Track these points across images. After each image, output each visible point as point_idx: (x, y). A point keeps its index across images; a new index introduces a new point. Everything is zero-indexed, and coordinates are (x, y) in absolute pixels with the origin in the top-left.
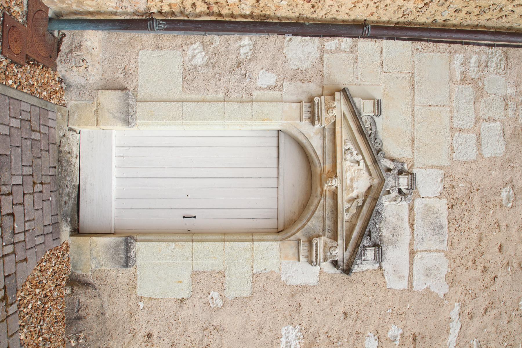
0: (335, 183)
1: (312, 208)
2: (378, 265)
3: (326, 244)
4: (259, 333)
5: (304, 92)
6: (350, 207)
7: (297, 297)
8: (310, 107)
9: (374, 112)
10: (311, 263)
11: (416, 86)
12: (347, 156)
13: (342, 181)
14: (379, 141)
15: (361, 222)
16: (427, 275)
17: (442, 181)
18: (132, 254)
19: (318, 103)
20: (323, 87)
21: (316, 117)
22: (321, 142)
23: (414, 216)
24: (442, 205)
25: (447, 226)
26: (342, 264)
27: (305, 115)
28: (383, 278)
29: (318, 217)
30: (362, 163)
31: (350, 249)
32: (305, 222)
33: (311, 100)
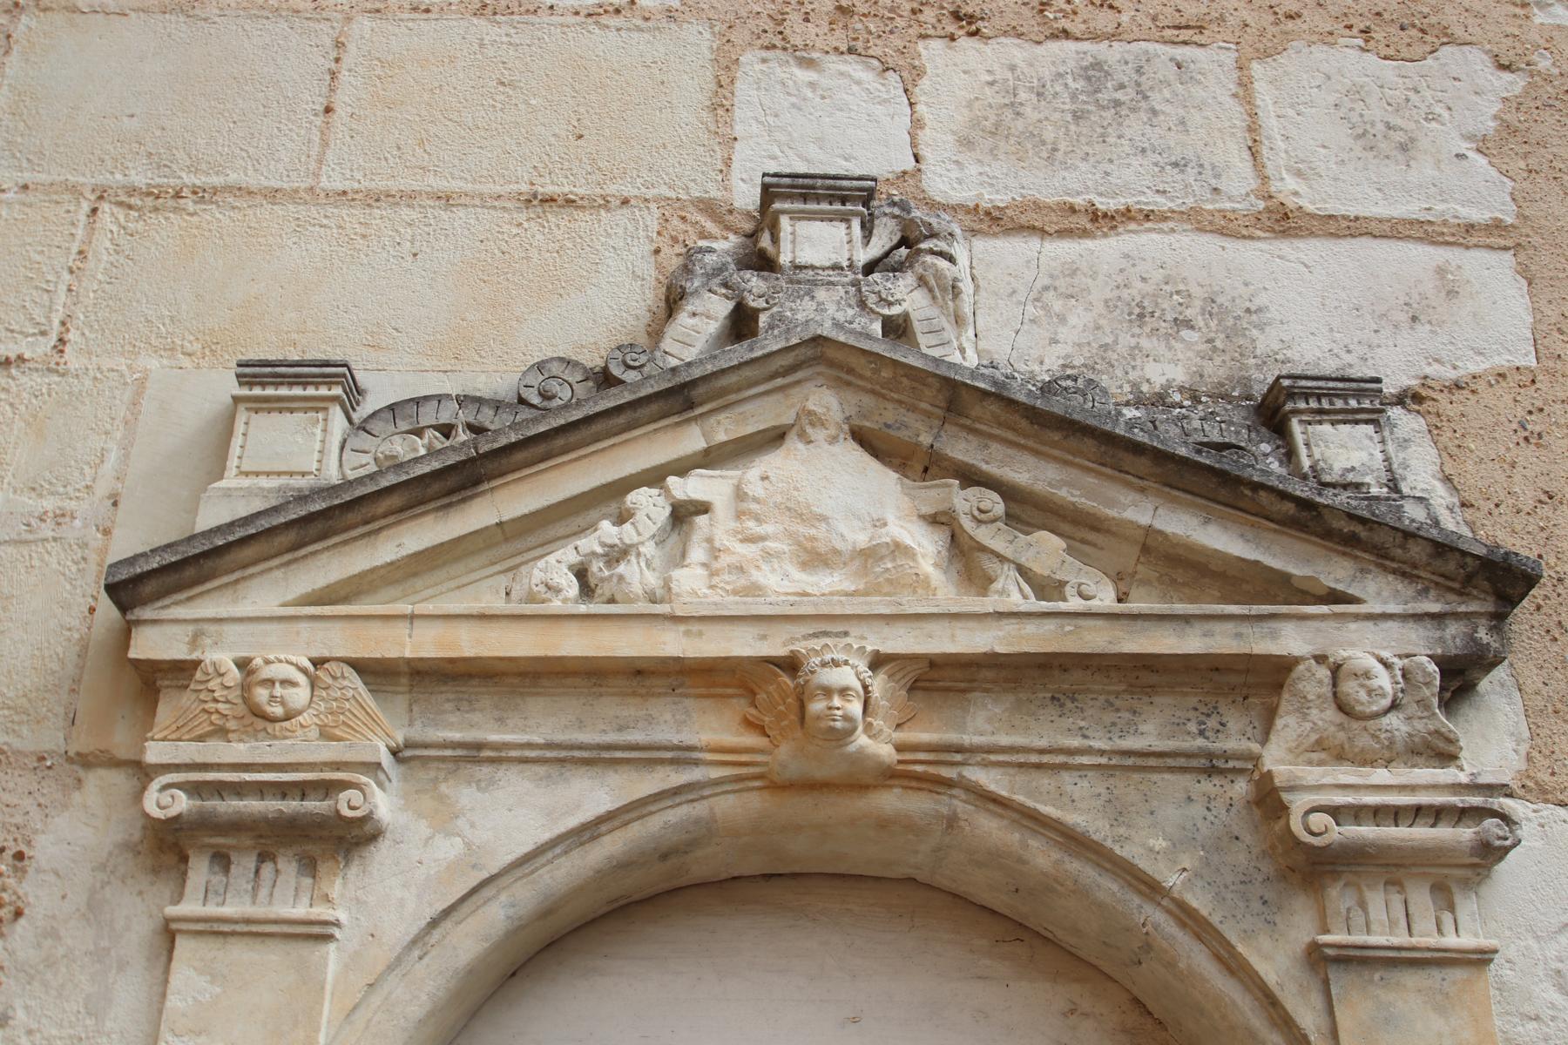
0: (843, 672)
1: (1042, 855)
2: (1395, 412)
3: (1319, 745)
5: (93, 908)
6: (1022, 570)
8: (222, 860)
9: (318, 405)
10: (1489, 854)
11: (189, 179)
12: (637, 589)
13: (829, 622)
14: (535, 379)
15: (1126, 497)
16: (1403, 148)
17: (808, 63)
19: (195, 789)
20: (86, 761)
21: (313, 805)
22: (514, 784)
23: (1037, 206)
25: (1086, 46)
26: (1453, 629)
27: (287, 896)
28: (1481, 386)
29: (1118, 813)
31: (1335, 572)
32: (1159, 917)
33: (168, 847)
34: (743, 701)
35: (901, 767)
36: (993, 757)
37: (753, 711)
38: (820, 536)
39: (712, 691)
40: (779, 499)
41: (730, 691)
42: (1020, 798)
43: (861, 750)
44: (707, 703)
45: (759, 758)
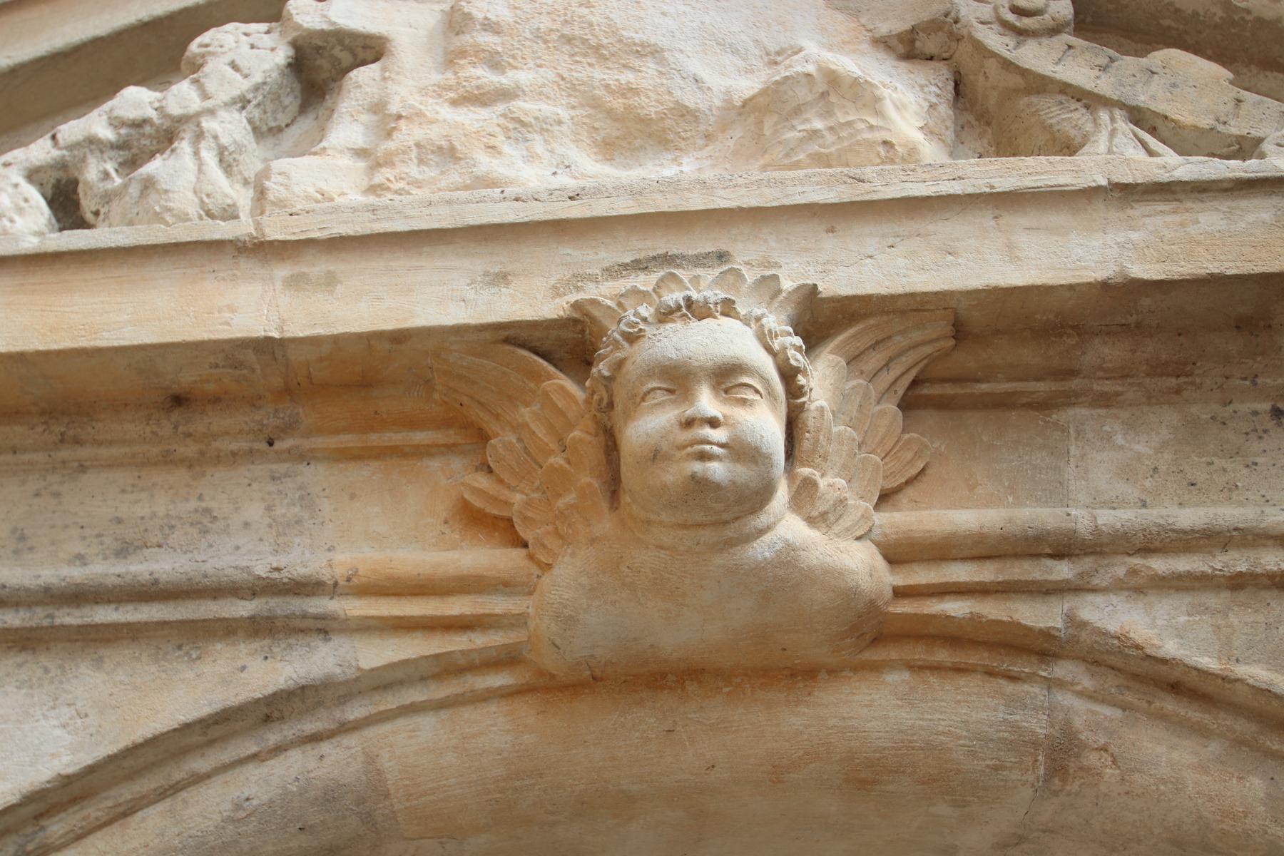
34: (457, 463)
35: (905, 607)
36: (1159, 565)
37: (482, 481)
38: (645, 83)
39: (374, 439)
40: (545, 23)
41: (420, 437)
42: (1256, 672)
43: (788, 558)
44: (360, 473)
45: (498, 605)
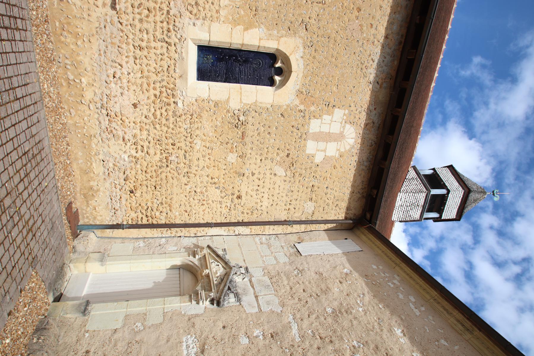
4: (168, 341)
7: (192, 320)
13: (211, 270)
18: (89, 308)
24: (266, 279)
30: (220, 265)
